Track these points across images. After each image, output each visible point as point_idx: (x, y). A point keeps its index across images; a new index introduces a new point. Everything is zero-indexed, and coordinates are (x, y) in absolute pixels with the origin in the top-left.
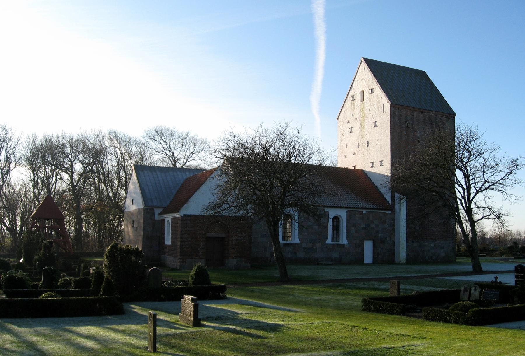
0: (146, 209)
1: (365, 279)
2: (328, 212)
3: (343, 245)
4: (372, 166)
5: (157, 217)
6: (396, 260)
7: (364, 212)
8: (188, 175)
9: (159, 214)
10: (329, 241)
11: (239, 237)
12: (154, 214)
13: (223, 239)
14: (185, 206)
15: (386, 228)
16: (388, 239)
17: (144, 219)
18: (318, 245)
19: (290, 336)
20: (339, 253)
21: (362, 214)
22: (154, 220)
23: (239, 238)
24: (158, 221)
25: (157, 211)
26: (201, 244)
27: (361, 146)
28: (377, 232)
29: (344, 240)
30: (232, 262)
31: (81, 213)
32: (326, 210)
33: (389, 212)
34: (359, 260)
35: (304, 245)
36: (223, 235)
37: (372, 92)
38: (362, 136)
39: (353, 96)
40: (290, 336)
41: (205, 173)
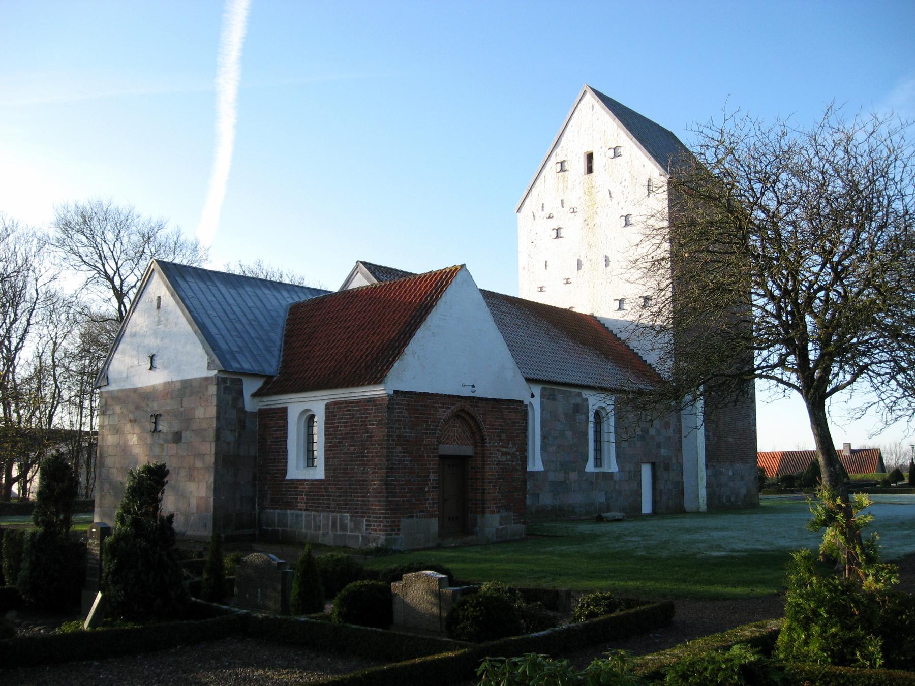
0: (224, 380)
2: (586, 400)
4: (620, 308)
5: (250, 404)
6: (688, 504)
8: (304, 298)
9: (254, 395)
10: (590, 467)
12: (241, 393)
13: (462, 460)
14: (396, 365)
15: (670, 438)
16: (674, 461)
17: (217, 406)
18: (573, 476)
20: (606, 493)
22: (242, 410)
23: (504, 458)
24: (252, 414)
25: (250, 386)
26: (432, 476)
27: (586, 265)
28: (659, 446)
29: (611, 465)
30: (493, 522)
31: (779, 302)
32: (585, 393)
34: (634, 512)
35: (552, 476)
36: (467, 450)
37: (616, 155)
38: (590, 246)
39: (562, 163)
41: (325, 297)
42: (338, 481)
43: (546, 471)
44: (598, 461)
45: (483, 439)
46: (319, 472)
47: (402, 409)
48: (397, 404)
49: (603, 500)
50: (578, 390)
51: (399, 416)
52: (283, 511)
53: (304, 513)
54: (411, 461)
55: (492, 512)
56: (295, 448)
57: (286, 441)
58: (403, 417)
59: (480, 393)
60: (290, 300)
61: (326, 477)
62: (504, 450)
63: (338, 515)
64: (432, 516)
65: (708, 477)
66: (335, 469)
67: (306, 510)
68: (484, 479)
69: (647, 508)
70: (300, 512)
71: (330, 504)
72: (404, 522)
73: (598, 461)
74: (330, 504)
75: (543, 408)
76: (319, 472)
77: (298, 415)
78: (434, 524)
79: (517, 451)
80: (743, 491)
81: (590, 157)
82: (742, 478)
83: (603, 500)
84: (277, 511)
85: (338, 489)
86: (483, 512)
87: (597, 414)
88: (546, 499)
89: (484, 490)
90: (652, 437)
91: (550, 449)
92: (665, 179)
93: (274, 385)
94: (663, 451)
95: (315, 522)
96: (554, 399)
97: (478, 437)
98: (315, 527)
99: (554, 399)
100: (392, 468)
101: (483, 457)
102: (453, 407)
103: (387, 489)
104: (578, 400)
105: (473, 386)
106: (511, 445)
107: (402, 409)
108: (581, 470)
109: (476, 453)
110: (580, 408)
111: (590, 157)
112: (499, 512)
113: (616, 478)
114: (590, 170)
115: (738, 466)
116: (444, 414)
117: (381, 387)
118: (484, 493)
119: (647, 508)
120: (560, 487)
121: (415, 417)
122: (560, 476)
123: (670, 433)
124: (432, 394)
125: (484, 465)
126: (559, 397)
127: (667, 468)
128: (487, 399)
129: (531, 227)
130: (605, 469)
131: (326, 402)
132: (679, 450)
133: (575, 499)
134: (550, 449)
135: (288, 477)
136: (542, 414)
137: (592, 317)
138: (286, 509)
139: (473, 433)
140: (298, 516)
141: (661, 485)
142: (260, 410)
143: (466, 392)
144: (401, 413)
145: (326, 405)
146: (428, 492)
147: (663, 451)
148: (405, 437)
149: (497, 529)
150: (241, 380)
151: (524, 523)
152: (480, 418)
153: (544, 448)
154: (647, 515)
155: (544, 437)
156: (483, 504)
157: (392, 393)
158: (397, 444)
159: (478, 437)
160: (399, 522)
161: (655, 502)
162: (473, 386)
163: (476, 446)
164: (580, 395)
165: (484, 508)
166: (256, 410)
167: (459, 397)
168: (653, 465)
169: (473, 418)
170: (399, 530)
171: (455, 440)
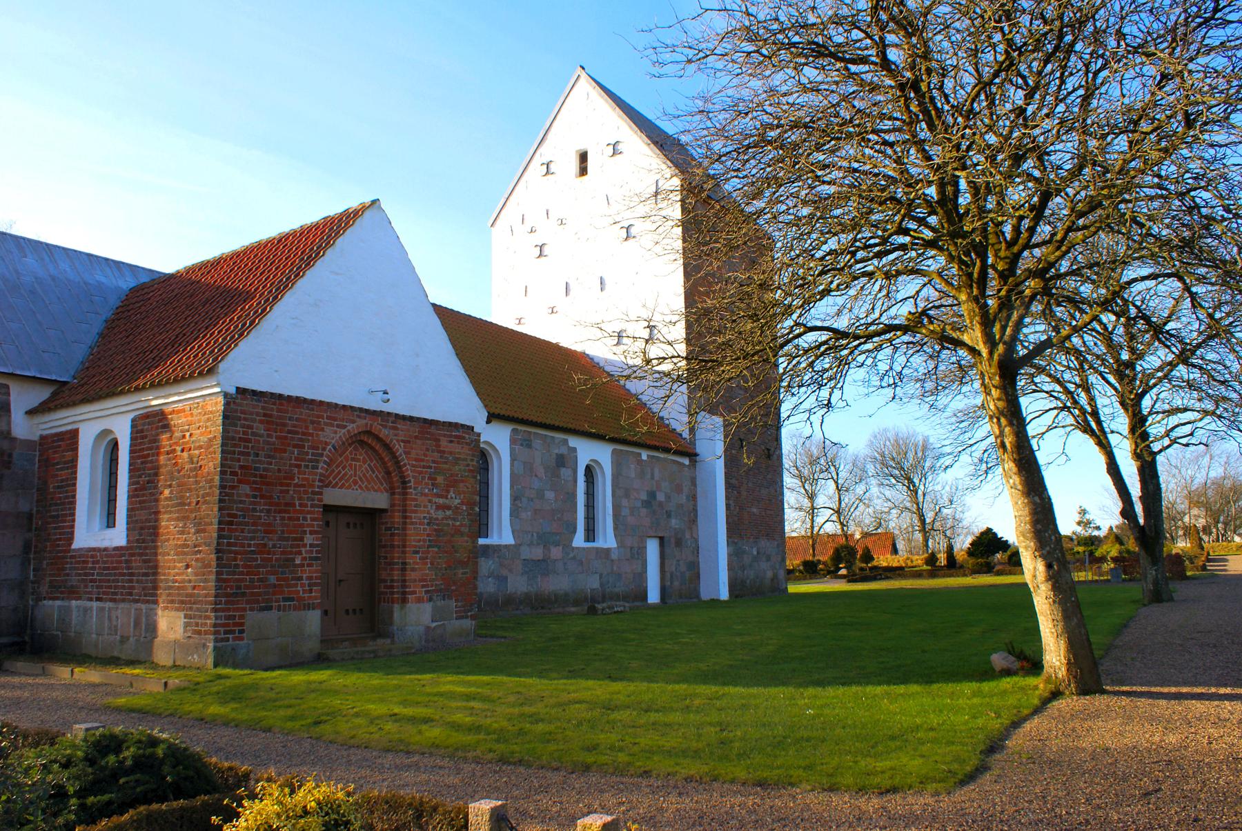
1: (1225, 695)
2: (574, 450)
3: (608, 550)
6: (705, 595)
7: (645, 455)
9: (31, 412)
10: (579, 541)
11: (439, 507)
13: (370, 516)
16: (688, 536)
18: (556, 552)
19: (349, 763)
21: (640, 462)
23: (440, 514)
24: (29, 444)
26: (309, 539)
28: (669, 515)
29: (607, 539)
30: (416, 617)
32: (574, 442)
33: (686, 461)
36: (378, 500)
40: (349, 763)
42: (146, 548)
43: (517, 546)
44: (590, 534)
45: (404, 482)
46: (118, 537)
47: (254, 421)
48: (243, 412)
49: (596, 585)
50: (559, 436)
51: (244, 433)
52: (66, 603)
53: (95, 604)
54: (269, 511)
55: (420, 600)
56: (86, 495)
57: (75, 485)
58: (254, 434)
59: (398, 406)
60: (127, 283)
61: (128, 541)
62: (441, 501)
63: (143, 606)
64: (308, 607)
65: (729, 555)
66: (142, 528)
67: (98, 599)
68: (404, 546)
69: (653, 597)
70: (89, 604)
71: (132, 588)
72: (253, 618)
73: (590, 534)
74: (132, 588)
75: (513, 459)
76: (118, 537)
77: (92, 440)
78: (313, 620)
79: (462, 503)
80: (769, 574)
81: (583, 157)
82: (768, 559)
83: (596, 585)
84: (58, 603)
85: (145, 561)
86: (404, 601)
87: (589, 470)
88: (518, 584)
89: (405, 563)
90: (661, 504)
91: (523, 515)
92: (676, 182)
93: (64, 395)
94: (674, 522)
95: (110, 617)
96: (529, 446)
97: (395, 479)
98: (110, 628)
99: (529, 446)
100: (231, 523)
101: (405, 511)
102: (350, 427)
103: (218, 559)
104: (563, 450)
105: (385, 393)
106: (452, 494)
107: (254, 421)
108: (567, 546)
109: (393, 505)
110: (565, 460)
111: (583, 157)
112: (430, 600)
113: (614, 556)
114: (583, 171)
115: (764, 543)
116: (332, 435)
117: (212, 381)
118: (404, 570)
119: (653, 597)
120: (541, 567)
121: (277, 437)
122: (538, 553)
123: (683, 499)
124: (313, 401)
125: (405, 523)
126: (537, 443)
127: (679, 543)
128: (411, 419)
129: (508, 243)
130: (600, 543)
131: (132, 415)
132: (693, 521)
133: (558, 584)
134: (523, 515)
135: (75, 546)
136: (512, 465)
137: (584, 355)
138: (70, 599)
139: (388, 473)
140: (86, 610)
141: (671, 566)
142: (42, 438)
143: (374, 404)
144: (251, 427)
145: (133, 421)
146: (302, 565)
147: (673, 521)
148: (256, 469)
149: (428, 628)
150: (8, 387)
151: (473, 618)
152: (399, 449)
153: (514, 513)
154: (654, 607)
155: (515, 498)
156: (404, 586)
157: (233, 391)
158: (240, 481)
159: (395, 479)
160: (242, 617)
161: (664, 591)
162: (385, 393)
163: (393, 494)
164: (566, 441)
165: (404, 593)
166: (36, 438)
167: (361, 410)
168: (661, 539)
169: (387, 447)
170: (242, 632)
171: (355, 483)
